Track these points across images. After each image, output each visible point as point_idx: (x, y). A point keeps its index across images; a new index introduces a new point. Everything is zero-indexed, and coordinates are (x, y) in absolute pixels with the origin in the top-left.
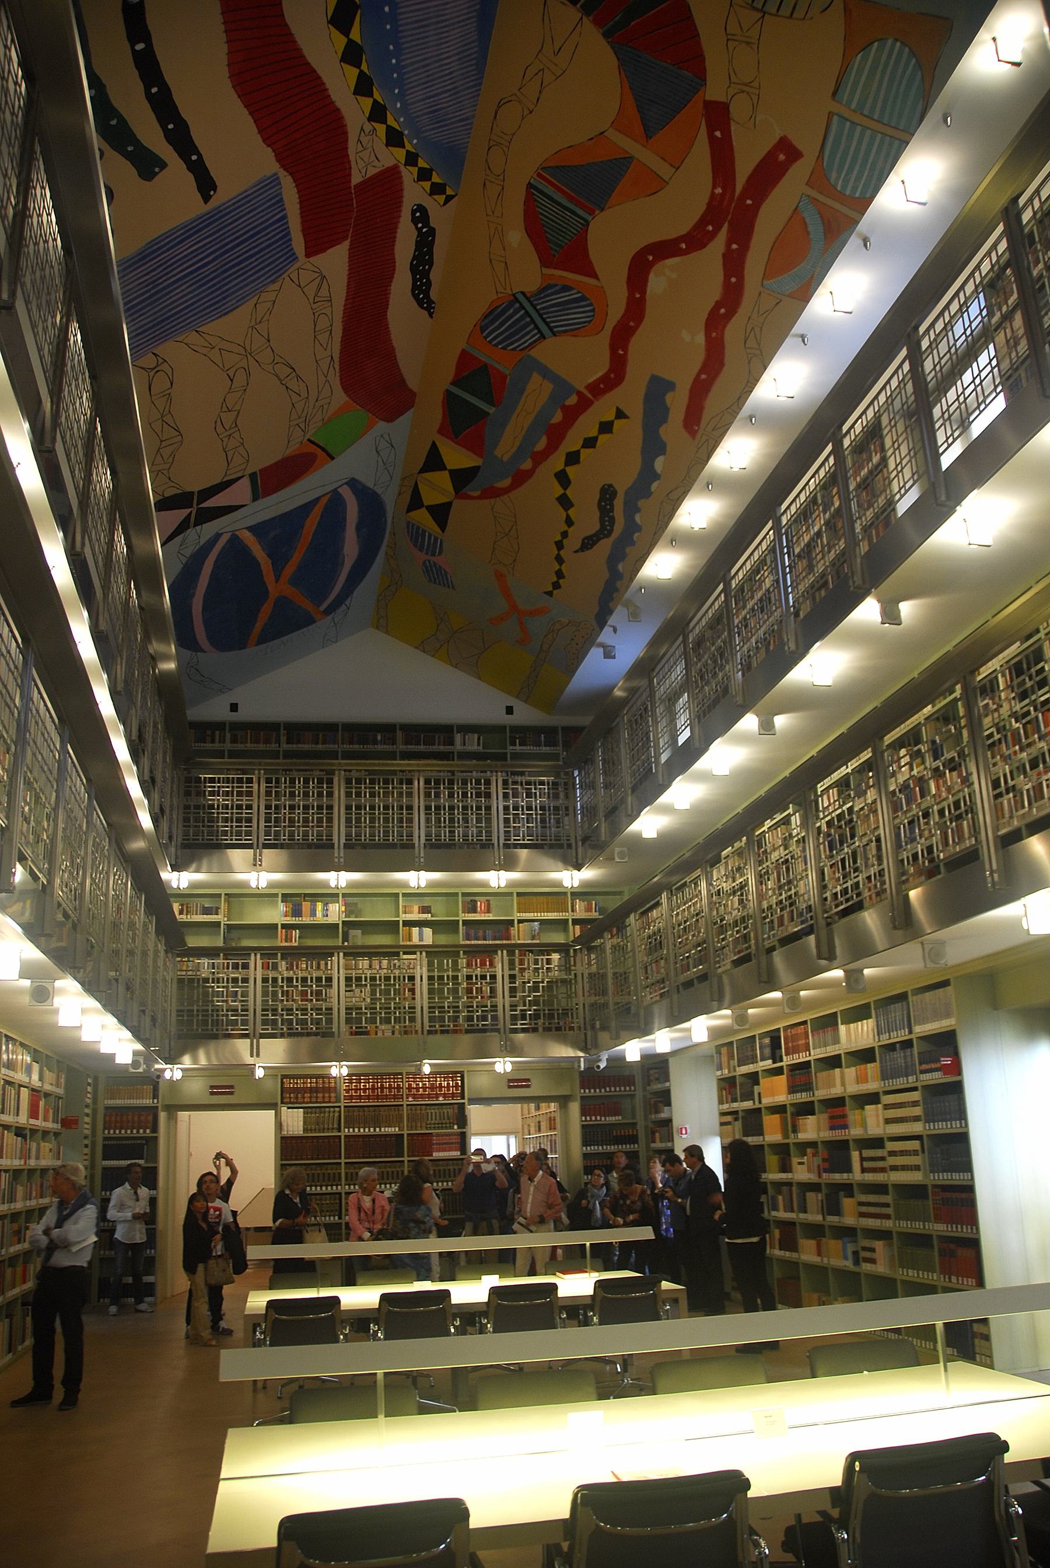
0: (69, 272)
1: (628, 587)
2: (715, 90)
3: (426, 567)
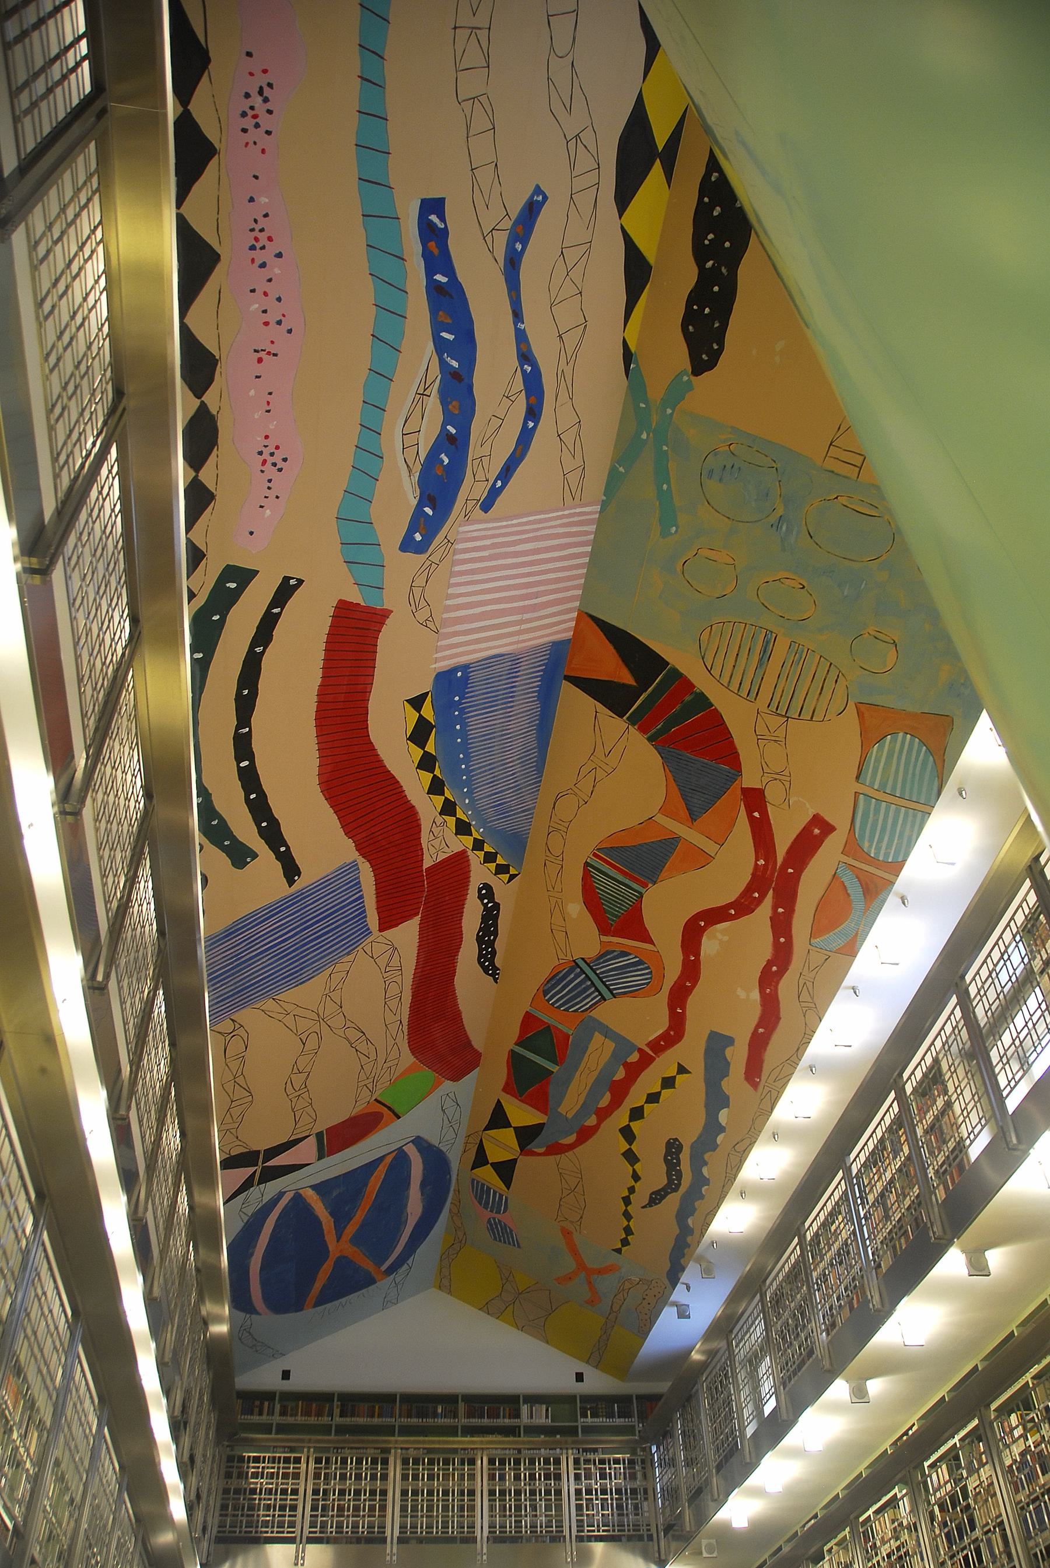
0: (160, 952)
1: (699, 1242)
2: (750, 779)
3: (491, 1225)
